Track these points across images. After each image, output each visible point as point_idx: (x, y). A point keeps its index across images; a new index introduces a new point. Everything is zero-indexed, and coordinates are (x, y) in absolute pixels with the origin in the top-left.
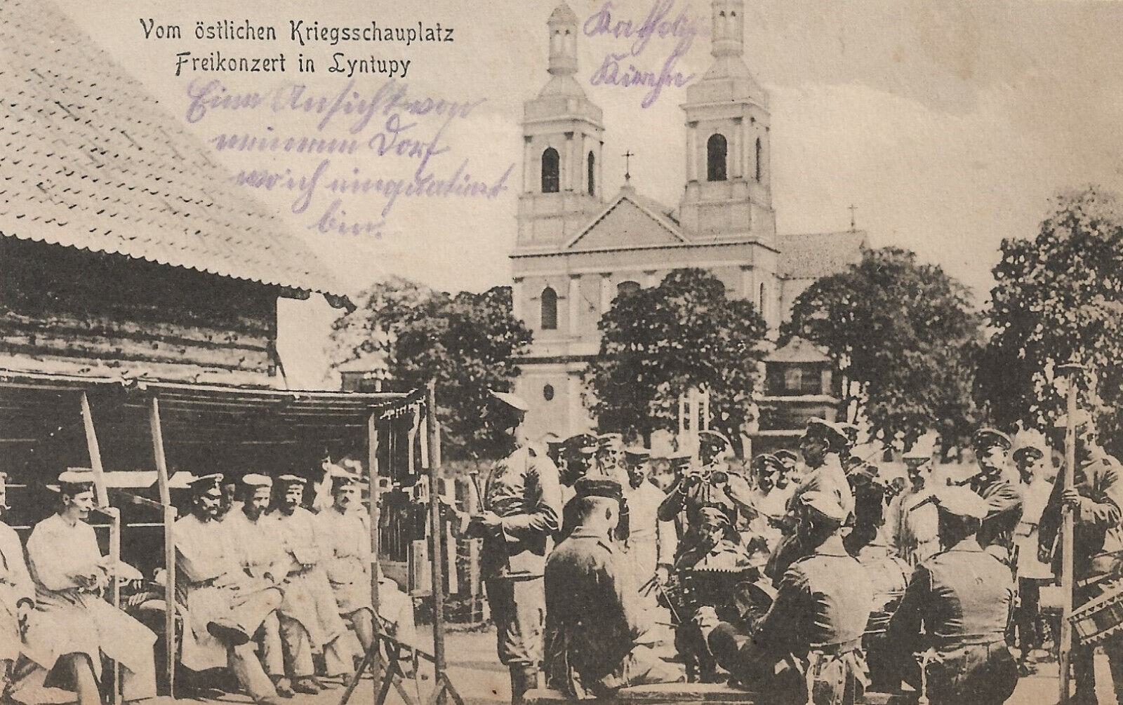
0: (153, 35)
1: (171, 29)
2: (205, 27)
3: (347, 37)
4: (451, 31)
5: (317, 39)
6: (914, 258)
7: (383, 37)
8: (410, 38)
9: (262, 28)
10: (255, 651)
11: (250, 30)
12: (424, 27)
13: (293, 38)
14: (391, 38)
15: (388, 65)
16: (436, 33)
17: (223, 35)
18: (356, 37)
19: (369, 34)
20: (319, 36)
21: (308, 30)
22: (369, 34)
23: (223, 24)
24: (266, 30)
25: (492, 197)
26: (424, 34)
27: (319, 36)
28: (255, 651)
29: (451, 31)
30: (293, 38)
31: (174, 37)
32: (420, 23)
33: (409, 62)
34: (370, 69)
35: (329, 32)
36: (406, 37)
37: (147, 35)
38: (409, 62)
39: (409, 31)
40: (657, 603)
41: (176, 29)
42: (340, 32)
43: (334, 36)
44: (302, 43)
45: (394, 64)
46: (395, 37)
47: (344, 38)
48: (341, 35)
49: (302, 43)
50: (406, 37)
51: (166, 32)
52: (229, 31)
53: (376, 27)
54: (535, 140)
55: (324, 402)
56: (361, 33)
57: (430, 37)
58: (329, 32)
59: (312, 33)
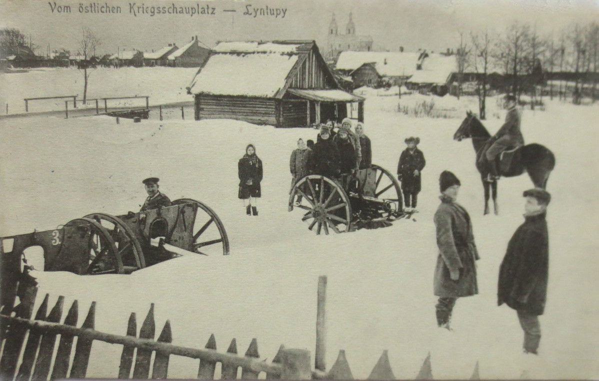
0: (56, 11)
1: (66, 8)
2: (84, 7)
6: (570, 99)
8: (277, 14)
10: (36, 279)
12: (200, 7)
18: (164, 12)
19: (104, 9)
21: (139, 8)
22: (104, 9)
23: (93, 5)
25: (544, 107)
26: (200, 10)
27: (145, 11)
28: (36, 279)
32: (198, 5)
36: (275, 13)
37: (53, 11)
39: (192, 9)
40: (171, 190)
42: (156, 9)
44: (135, 15)
46: (184, 12)
48: (156, 11)
49: (135, 15)
50: (275, 13)
52: (96, 9)
56: (166, 9)
59: (141, 10)
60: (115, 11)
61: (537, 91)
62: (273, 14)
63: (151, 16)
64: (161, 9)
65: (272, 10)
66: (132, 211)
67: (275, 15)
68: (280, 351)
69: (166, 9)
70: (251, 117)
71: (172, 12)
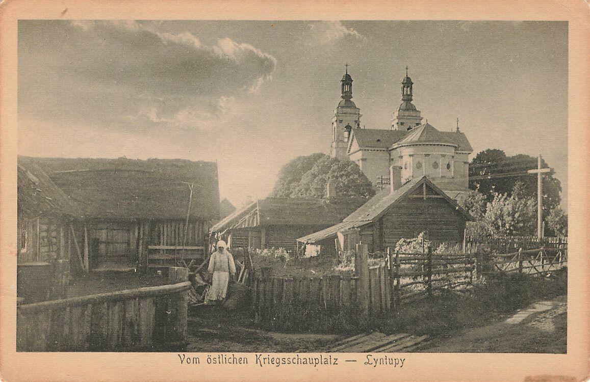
1: (195, 359)
3: (284, 362)
4: (337, 359)
5: (269, 363)
7: (302, 363)
9: (241, 358)
11: (235, 359)
13: (257, 363)
14: (306, 363)
15: (394, 361)
16: (329, 360)
17: (221, 362)
20: (270, 362)
22: (295, 361)
24: (243, 359)
26: (323, 360)
27: (270, 362)
29: (337, 359)
30: (257, 363)
31: (196, 363)
33: (404, 360)
34: (385, 363)
35: (275, 360)
36: (314, 362)
38: (404, 360)
41: (197, 359)
42: (281, 360)
43: (278, 362)
45: (397, 360)
46: (308, 362)
47: (283, 363)
48: (281, 361)
50: (314, 362)
51: (192, 361)
53: (235, 357)
54: (343, 122)
55: (217, 193)
56: (291, 360)
57: (305, 362)
58: (275, 360)
59: (266, 361)
60: (242, 362)
61: (569, 196)
62: (392, 364)
63: (277, 366)
64: (286, 360)
65: (311, 360)
66: (228, 199)
67: (314, 364)
68: (19, 162)
69: (291, 360)
70: (439, 197)
71: (232, 362)
